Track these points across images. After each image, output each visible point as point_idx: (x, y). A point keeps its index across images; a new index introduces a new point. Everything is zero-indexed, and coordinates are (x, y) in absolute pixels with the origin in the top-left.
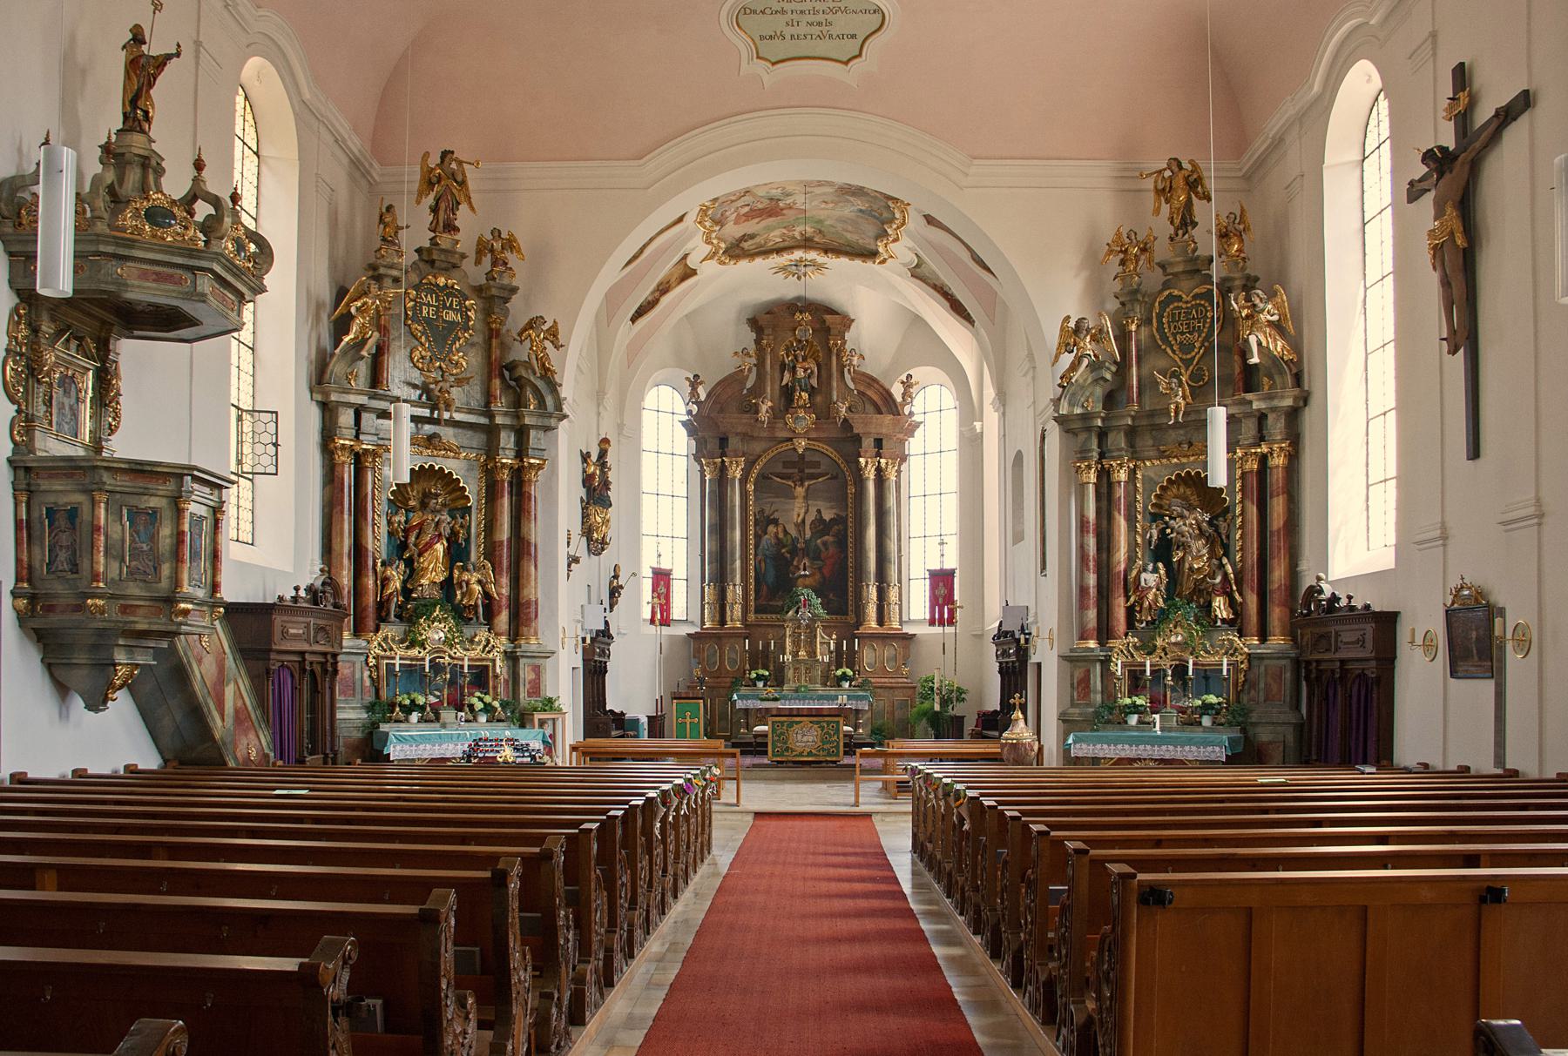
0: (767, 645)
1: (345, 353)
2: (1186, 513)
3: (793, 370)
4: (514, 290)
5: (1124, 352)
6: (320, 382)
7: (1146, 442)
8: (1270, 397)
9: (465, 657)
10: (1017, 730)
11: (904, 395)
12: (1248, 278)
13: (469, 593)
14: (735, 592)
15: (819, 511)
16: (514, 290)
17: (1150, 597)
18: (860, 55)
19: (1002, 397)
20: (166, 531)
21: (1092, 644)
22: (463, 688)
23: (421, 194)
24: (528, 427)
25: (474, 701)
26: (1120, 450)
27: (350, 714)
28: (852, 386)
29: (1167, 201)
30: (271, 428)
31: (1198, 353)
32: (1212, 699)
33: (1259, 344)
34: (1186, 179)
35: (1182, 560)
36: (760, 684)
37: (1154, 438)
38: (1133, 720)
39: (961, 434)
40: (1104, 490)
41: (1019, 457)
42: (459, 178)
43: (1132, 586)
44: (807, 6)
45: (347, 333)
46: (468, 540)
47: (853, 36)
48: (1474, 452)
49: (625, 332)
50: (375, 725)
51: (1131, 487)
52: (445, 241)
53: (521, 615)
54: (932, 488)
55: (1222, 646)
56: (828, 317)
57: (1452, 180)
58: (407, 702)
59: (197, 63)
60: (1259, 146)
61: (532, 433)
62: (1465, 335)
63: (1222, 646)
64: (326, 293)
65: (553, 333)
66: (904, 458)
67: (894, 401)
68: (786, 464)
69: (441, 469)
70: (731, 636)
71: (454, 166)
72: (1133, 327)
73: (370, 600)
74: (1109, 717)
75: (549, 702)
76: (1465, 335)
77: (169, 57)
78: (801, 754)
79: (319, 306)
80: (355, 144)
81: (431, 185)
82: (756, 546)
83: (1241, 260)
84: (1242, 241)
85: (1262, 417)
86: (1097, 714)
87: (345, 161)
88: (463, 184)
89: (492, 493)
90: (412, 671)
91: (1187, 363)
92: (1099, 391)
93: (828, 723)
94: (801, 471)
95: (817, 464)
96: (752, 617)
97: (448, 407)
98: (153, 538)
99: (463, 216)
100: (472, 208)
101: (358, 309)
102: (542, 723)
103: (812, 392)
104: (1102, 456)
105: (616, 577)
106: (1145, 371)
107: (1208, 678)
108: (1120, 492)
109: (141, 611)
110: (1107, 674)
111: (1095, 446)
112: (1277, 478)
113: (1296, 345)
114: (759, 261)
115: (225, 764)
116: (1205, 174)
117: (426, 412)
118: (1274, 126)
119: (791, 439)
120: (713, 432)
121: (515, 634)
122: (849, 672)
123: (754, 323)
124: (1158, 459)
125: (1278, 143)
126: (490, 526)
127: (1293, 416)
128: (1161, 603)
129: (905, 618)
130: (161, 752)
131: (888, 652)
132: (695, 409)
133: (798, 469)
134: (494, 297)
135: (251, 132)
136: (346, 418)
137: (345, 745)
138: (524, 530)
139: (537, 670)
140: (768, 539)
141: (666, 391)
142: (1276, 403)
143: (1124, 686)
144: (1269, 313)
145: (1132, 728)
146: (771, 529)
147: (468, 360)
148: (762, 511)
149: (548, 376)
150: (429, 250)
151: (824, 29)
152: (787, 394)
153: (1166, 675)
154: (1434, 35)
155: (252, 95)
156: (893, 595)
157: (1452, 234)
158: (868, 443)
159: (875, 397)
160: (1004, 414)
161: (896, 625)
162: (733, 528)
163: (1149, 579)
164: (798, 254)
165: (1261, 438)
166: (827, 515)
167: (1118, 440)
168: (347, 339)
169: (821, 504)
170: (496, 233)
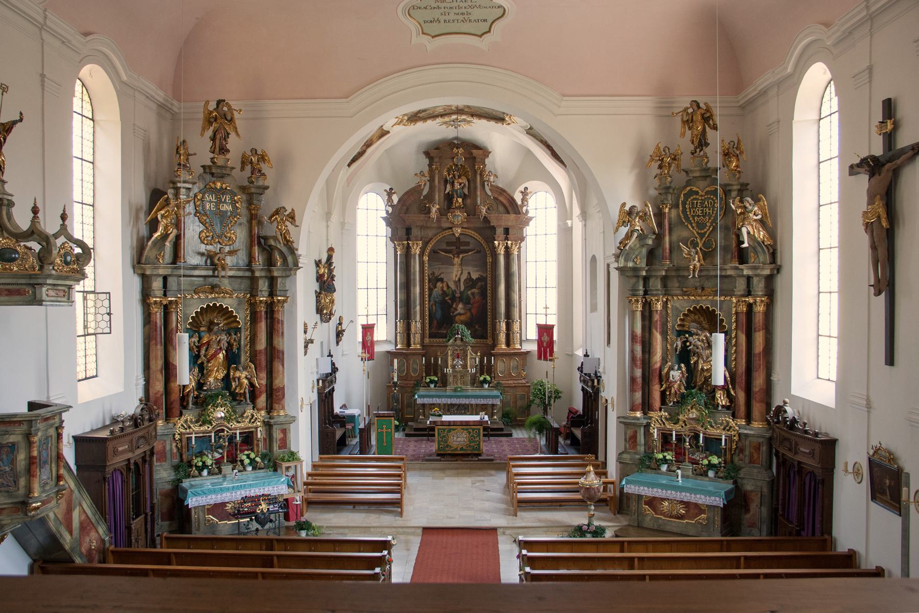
0: (436, 360)
1: (155, 243)
2: (700, 332)
3: (453, 184)
4: (267, 188)
5: (660, 225)
6: (139, 262)
7: (674, 284)
8: (755, 268)
9: (237, 427)
10: (590, 479)
11: (523, 200)
12: (742, 185)
13: (240, 385)
14: (416, 326)
15: (469, 273)
16: (267, 188)
17: (676, 386)
18: (489, 31)
19: (584, 215)
20: (21, 457)
21: (639, 414)
22: (236, 449)
23: (204, 130)
24: (277, 277)
25: (244, 457)
26: (657, 290)
27: (163, 474)
28: (490, 194)
29: (690, 128)
30: (106, 303)
31: (708, 229)
32: (715, 460)
33: (748, 233)
34: (702, 115)
35: (696, 363)
36: (432, 386)
37: (679, 282)
38: (664, 468)
39: (559, 226)
40: (647, 314)
41: (594, 259)
42: (229, 118)
43: (663, 378)
44: (455, 4)
45: (156, 231)
46: (239, 349)
47: (485, 20)
48: (890, 360)
49: (344, 173)
50: (180, 481)
51: (664, 312)
52: (220, 161)
53: (274, 396)
54: (541, 292)
55: (721, 424)
56: (475, 152)
57: (879, 172)
58: (200, 464)
59: (43, 89)
60: (751, 92)
61: (279, 280)
62: (886, 284)
63: (721, 424)
64: (141, 197)
65: (292, 217)
66: (522, 239)
67: (516, 204)
68: (448, 244)
69: (221, 305)
70: (413, 354)
71: (225, 109)
72: (667, 210)
73: (175, 396)
74: (648, 463)
75: (293, 454)
76: (886, 284)
77: (14, 123)
78: (456, 449)
79: (138, 211)
80: (160, 95)
81: (211, 124)
82: (430, 295)
83: (737, 171)
84: (738, 160)
85: (749, 278)
86: (642, 461)
87: (154, 106)
88: (231, 120)
89: (254, 318)
90: (203, 439)
91: (702, 236)
92: (644, 251)
93: (473, 430)
94: (458, 248)
95: (468, 244)
96: (427, 340)
97: (224, 269)
98: (13, 462)
99: (233, 143)
100: (238, 135)
101: (163, 216)
102: (288, 468)
103: (464, 197)
104: (646, 293)
105: (340, 324)
106: (674, 238)
107: (712, 444)
108: (656, 317)
109: (6, 512)
110: (648, 434)
111: (641, 288)
112: (759, 319)
113: (772, 233)
114: (429, 122)
115: (73, 562)
116: (714, 112)
117: (210, 273)
118: (761, 83)
119: (451, 228)
120: (404, 222)
121: (270, 409)
122: (488, 378)
123: (427, 154)
124: (682, 295)
125: (764, 93)
126: (253, 340)
127: (770, 280)
128: (683, 390)
129: (524, 338)
130: (29, 555)
131: (513, 363)
132: (390, 210)
133: (456, 246)
134: (252, 193)
135: (87, 106)
136: (157, 284)
137: (160, 494)
138: (275, 342)
139: (284, 432)
140: (437, 291)
141: (372, 196)
142: (759, 272)
143: (658, 444)
144: (755, 212)
145: (662, 474)
146: (439, 284)
147: (239, 235)
148: (433, 274)
149: (289, 244)
150: (210, 167)
151: (466, 17)
152: (449, 198)
153: (685, 441)
154: (870, 69)
155: (86, 82)
156: (516, 327)
157: (879, 217)
158: (500, 231)
159: (505, 202)
160: (585, 225)
161: (518, 346)
162: (415, 286)
163: (676, 375)
164: (454, 117)
165: (749, 293)
166: (475, 276)
167: (656, 284)
168: (156, 235)
169: (471, 269)
170: (254, 151)
